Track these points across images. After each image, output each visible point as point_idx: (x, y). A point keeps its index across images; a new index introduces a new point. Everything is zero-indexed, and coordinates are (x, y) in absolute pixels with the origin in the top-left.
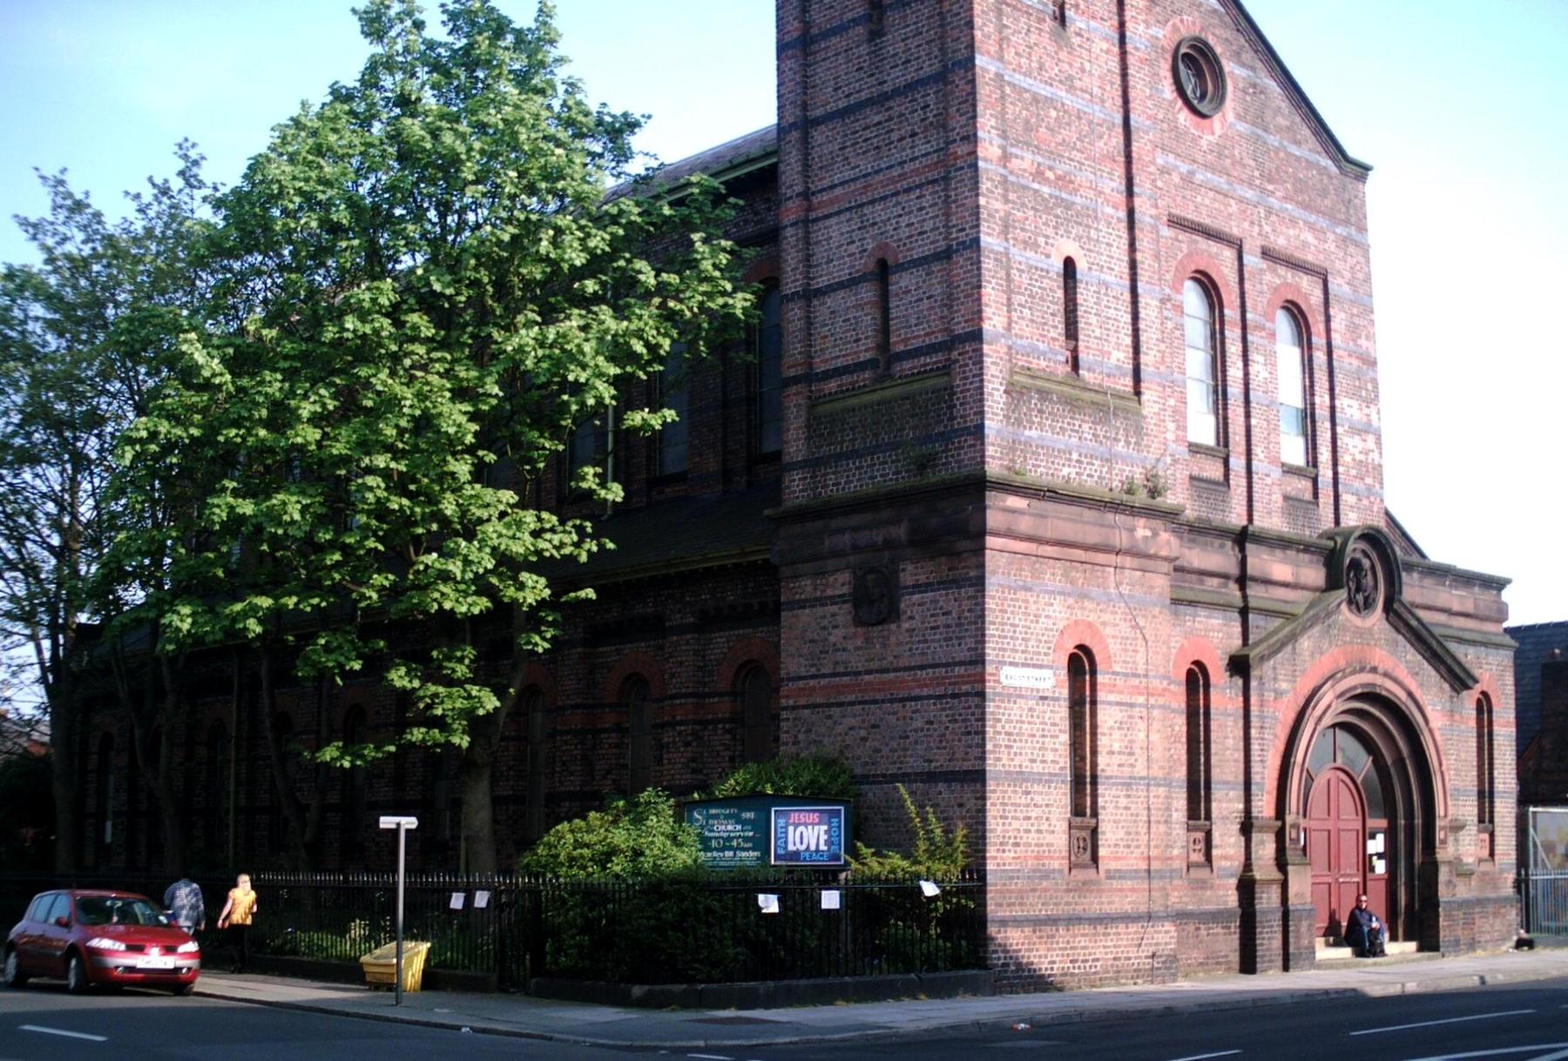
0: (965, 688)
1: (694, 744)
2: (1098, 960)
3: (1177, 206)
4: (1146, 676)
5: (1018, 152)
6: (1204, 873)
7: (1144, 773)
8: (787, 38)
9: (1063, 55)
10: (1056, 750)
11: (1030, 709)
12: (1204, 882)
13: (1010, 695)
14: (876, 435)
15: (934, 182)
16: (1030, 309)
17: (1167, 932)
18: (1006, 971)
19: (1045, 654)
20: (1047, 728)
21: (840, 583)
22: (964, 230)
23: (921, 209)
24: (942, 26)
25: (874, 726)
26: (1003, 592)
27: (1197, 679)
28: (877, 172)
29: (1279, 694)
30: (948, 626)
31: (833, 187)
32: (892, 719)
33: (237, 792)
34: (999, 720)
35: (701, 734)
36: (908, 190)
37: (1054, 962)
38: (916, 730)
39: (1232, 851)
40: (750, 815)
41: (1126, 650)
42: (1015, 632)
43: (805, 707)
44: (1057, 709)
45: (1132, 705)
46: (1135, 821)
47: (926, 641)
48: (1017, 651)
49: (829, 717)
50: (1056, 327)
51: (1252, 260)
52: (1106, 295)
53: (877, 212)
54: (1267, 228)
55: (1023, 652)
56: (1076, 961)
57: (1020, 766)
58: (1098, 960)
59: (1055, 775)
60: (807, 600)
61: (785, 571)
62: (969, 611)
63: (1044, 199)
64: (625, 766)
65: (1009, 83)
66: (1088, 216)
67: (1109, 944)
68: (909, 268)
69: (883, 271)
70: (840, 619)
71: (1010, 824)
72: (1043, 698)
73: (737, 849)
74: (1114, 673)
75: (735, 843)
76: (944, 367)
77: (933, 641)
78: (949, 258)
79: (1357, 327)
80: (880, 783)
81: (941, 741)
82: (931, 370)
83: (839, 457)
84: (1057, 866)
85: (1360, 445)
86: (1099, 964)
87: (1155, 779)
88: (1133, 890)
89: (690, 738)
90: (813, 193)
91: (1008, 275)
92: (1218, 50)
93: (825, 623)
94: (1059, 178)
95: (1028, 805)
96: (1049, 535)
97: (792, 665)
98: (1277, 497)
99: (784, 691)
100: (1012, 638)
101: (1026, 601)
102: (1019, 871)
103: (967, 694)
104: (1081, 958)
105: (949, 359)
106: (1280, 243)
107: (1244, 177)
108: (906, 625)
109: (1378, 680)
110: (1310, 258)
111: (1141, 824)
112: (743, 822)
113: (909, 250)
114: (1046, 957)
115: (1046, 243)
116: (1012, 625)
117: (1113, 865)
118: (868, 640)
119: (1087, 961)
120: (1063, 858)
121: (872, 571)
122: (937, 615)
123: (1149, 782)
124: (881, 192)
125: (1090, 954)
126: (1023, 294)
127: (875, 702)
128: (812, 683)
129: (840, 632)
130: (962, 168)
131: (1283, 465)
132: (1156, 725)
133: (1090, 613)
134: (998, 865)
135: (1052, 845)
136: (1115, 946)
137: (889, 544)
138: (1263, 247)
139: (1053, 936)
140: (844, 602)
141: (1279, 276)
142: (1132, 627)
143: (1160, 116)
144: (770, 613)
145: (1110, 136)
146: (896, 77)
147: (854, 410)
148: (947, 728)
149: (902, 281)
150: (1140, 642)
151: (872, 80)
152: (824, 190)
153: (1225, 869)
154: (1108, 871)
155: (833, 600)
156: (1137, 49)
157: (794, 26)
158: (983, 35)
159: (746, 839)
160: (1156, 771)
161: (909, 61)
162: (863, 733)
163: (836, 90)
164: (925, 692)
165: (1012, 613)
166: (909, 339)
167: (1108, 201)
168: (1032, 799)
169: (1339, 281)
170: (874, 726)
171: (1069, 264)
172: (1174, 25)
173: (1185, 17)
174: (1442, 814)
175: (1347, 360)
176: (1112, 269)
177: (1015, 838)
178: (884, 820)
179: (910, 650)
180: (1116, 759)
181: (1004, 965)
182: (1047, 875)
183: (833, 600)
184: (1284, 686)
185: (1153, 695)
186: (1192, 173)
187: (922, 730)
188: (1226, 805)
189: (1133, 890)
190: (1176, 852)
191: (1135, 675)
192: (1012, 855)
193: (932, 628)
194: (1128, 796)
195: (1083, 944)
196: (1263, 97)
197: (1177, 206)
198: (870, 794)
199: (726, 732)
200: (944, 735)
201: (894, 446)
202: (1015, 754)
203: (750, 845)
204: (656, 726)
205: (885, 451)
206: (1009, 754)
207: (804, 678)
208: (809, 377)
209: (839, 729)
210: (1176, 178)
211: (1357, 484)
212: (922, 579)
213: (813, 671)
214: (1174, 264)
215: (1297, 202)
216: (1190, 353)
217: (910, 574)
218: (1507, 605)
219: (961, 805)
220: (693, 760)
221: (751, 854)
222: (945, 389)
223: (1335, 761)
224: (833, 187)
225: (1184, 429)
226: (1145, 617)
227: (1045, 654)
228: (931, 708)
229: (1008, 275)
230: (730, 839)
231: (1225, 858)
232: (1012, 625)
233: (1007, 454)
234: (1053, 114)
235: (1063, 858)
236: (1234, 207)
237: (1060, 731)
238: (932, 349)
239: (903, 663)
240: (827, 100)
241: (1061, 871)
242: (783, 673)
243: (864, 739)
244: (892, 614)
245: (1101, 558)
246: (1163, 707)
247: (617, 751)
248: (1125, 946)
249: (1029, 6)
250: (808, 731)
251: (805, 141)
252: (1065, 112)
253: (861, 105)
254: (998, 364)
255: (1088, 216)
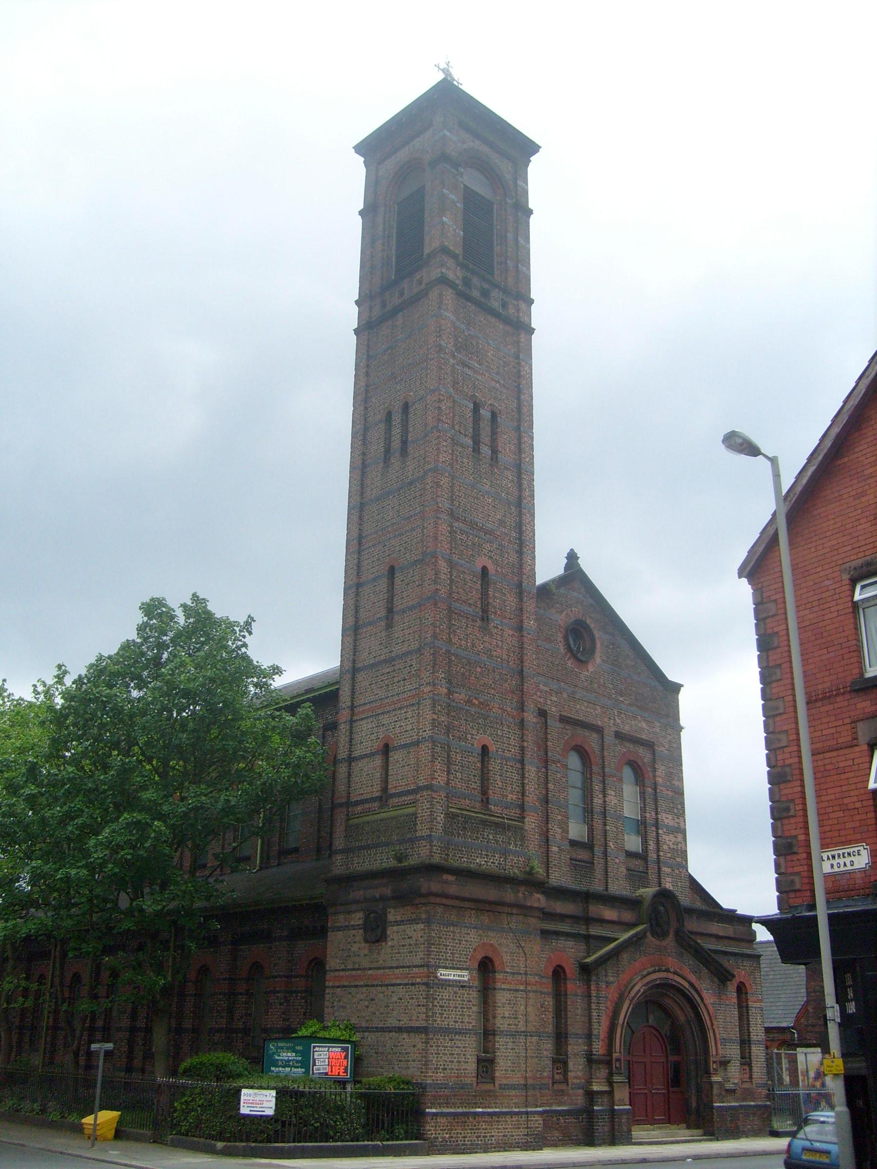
0: (418, 980)
1: (285, 1004)
2: (493, 1136)
3: (565, 711)
4: (526, 974)
5: (458, 690)
6: (562, 1087)
7: (523, 1029)
8: (347, 626)
9: (486, 638)
10: (470, 1016)
11: (455, 993)
12: (563, 1091)
13: (443, 985)
14: (379, 837)
15: (413, 705)
16: (461, 773)
17: (537, 1121)
18: (436, 1142)
19: (465, 962)
20: (464, 1003)
21: (358, 918)
22: (425, 731)
23: (406, 719)
24: (420, 624)
25: (372, 1000)
26: (440, 927)
27: (558, 973)
28: (386, 698)
29: (608, 984)
30: (410, 945)
31: (365, 704)
32: (381, 995)
33: (49, 1018)
34: (436, 999)
35: (288, 999)
36: (401, 708)
37: (465, 1137)
38: (392, 1003)
39: (580, 1074)
40: (299, 1048)
41: (513, 960)
42: (446, 949)
43: (338, 987)
44: (471, 992)
45: (517, 990)
46: (517, 1056)
47: (399, 953)
48: (448, 960)
49: (350, 993)
50: (476, 783)
51: (609, 739)
52: (505, 765)
53: (385, 719)
54: (618, 721)
55: (451, 960)
56: (480, 1136)
57: (448, 1025)
58: (493, 1136)
59: (469, 1030)
60: (341, 927)
61: (331, 910)
62: (421, 937)
63: (471, 714)
64: (250, 1015)
65: (454, 654)
66: (497, 723)
67: (500, 1127)
68: (399, 749)
69: (386, 750)
70: (357, 938)
71: (441, 1057)
72: (463, 987)
73: (292, 1067)
74: (506, 972)
75: (291, 1063)
76: (414, 803)
77: (403, 953)
78: (418, 745)
79: (671, 773)
80: (374, 1032)
81: (405, 1010)
82: (407, 804)
83: (361, 848)
84: (469, 1082)
85: (673, 839)
86: (493, 1139)
87: (530, 1032)
88: (516, 1096)
89: (282, 1001)
90: (356, 707)
91: (449, 755)
92: (592, 626)
93: (349, 940)
94: (481, 703)
95: (452, 1047)
96: (467, 895)
97: (332, 963)
98: (623, 870)
99: (328, 977)
100: (444, 953)
101: (454, 932)
102: (446, 1084)
103: (419, 983)
104: (482, 1135)
105: (415, 799)
106: (626, 729)
107: (605, 693)
108: (390, 944)
109: (671, 976)
110: (644, 737)
111: (522, 1058)
112: (296, 1052)
113: (400, 739)
114: (461, 1134)
115: (472, 738)
116: (444, 945)
117: (504, 1082)
118: (370, 950)
119: (486, 1137)
120: (473, 1077)
121: (373, 912)
122: (405, 938)
123: (526, 1034)
124: (388, 708)
125: (488, 1133)
126: (457, 765)
127: (373, 986)
128: (342, 973)
129: (357, 945)
130: (426, 699)
131: (627, 852)
132: (531, 1002)
133: (493, 938)
134: (433, 1080)
135: (467, 1069)
136: (504, 1129)
137: (382, 898)
138: (616, 732)
139: (466, 1122)
140: (359, 929)
141: (626, 747)
142: (518, 947)
143: (557, 663)
144: (322, 932)
145: (511, 680)
146: (398, 650)
147: (368, 822)
148: (408, 1002)
149: (395, 756)
150: (522, 955)
151: (387, 650)
152: (361, 705)
153: (576, 1084)
154: (500, 1085)
155: (354, 927)
156: (529, 634)
157: (351, 620)
158: (439, 630)
159: (297, 1061)
160: (531, 1028)
161: (404, 641)
162: (366, 1003)
163: (369, 654)
164: (398, 982)
165: (445, 938)
166: (397, 786)
167: (509, 715)
168: (455, 1044)
169: (662, 749)
170: (372, 1000)
171: (485, 749)
172: (567, 614)
173: (573, 609)
174: (714, 1053)
175: (666, 792)
176: (510, 751)
177: (444, 1065)
178: (376, 1053)
179: (392, 957)
180: (507, 1021)
181: (435, 1138)
182: (463, 1086)
183: (354, 927)
184: (612, 979)
185: (530, 984)
186: (574, 693)
187: (396, 1003)
188: (576, 1047)
189: (516, 1096)
190: (545, 1074)
191: (518, 974)
192: (442, 1075)
193: (403, 946)
194: (514, 1042)
195: (484, 1127)
196: (618, 650)
197: (565, 711)
198: (369, 1038)
199: (304, 998)
200: (407, 1006)
201: (387, 844)
202: (445, 1018)
203: (300, 1064)
204: (267, 993)
205: (382, 847)
206: (441, 1018)
207: (338, 970)
208: (348, 804)
209: (355, 1000)
210: (565, 695)
211: (670, 861)
212: (399, 918)
213: (343, 967)
214: (563, 741)
215: (637, 706)
216: (571, 791)
217: (392, 915)
218: (755, 932)
219: (414, 1046)
220: (284, 1013)
221: (300, 1069)
222: (413, 814)
223: (648, 1021)
224: (365, 704)
225: (567, 832)
226: (525, 941)
227: (465, 962)
228: (400, 990)
229: (449, 755)
230: (289, 1061)
231: (576, 1078)
232: (444, 945)
233: (444, 851)
234: (479, 670)
235: (473, 1077)
236: (599, 710)
237: (473, 1005)
238: (409, 792)
239: (389, 964)
240: (365, 658)
241: (471, 1084)
242: (327, 968)
243: (367, 1007)
244: (382, 938)
245: (499, 908)
246: (536, 991)
247: (247, 1006)
248: (511, 1129)
249: (467, 614)
250: (339, 1001)
251: (353, 679)
252: (486, 668)
253: (380, 663)
254: (440, 803)
255: (497, 723)
